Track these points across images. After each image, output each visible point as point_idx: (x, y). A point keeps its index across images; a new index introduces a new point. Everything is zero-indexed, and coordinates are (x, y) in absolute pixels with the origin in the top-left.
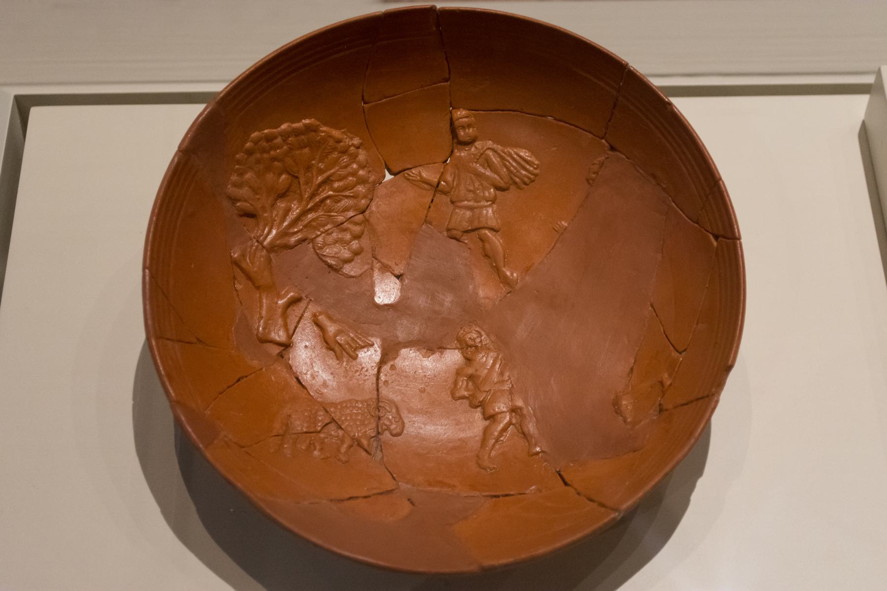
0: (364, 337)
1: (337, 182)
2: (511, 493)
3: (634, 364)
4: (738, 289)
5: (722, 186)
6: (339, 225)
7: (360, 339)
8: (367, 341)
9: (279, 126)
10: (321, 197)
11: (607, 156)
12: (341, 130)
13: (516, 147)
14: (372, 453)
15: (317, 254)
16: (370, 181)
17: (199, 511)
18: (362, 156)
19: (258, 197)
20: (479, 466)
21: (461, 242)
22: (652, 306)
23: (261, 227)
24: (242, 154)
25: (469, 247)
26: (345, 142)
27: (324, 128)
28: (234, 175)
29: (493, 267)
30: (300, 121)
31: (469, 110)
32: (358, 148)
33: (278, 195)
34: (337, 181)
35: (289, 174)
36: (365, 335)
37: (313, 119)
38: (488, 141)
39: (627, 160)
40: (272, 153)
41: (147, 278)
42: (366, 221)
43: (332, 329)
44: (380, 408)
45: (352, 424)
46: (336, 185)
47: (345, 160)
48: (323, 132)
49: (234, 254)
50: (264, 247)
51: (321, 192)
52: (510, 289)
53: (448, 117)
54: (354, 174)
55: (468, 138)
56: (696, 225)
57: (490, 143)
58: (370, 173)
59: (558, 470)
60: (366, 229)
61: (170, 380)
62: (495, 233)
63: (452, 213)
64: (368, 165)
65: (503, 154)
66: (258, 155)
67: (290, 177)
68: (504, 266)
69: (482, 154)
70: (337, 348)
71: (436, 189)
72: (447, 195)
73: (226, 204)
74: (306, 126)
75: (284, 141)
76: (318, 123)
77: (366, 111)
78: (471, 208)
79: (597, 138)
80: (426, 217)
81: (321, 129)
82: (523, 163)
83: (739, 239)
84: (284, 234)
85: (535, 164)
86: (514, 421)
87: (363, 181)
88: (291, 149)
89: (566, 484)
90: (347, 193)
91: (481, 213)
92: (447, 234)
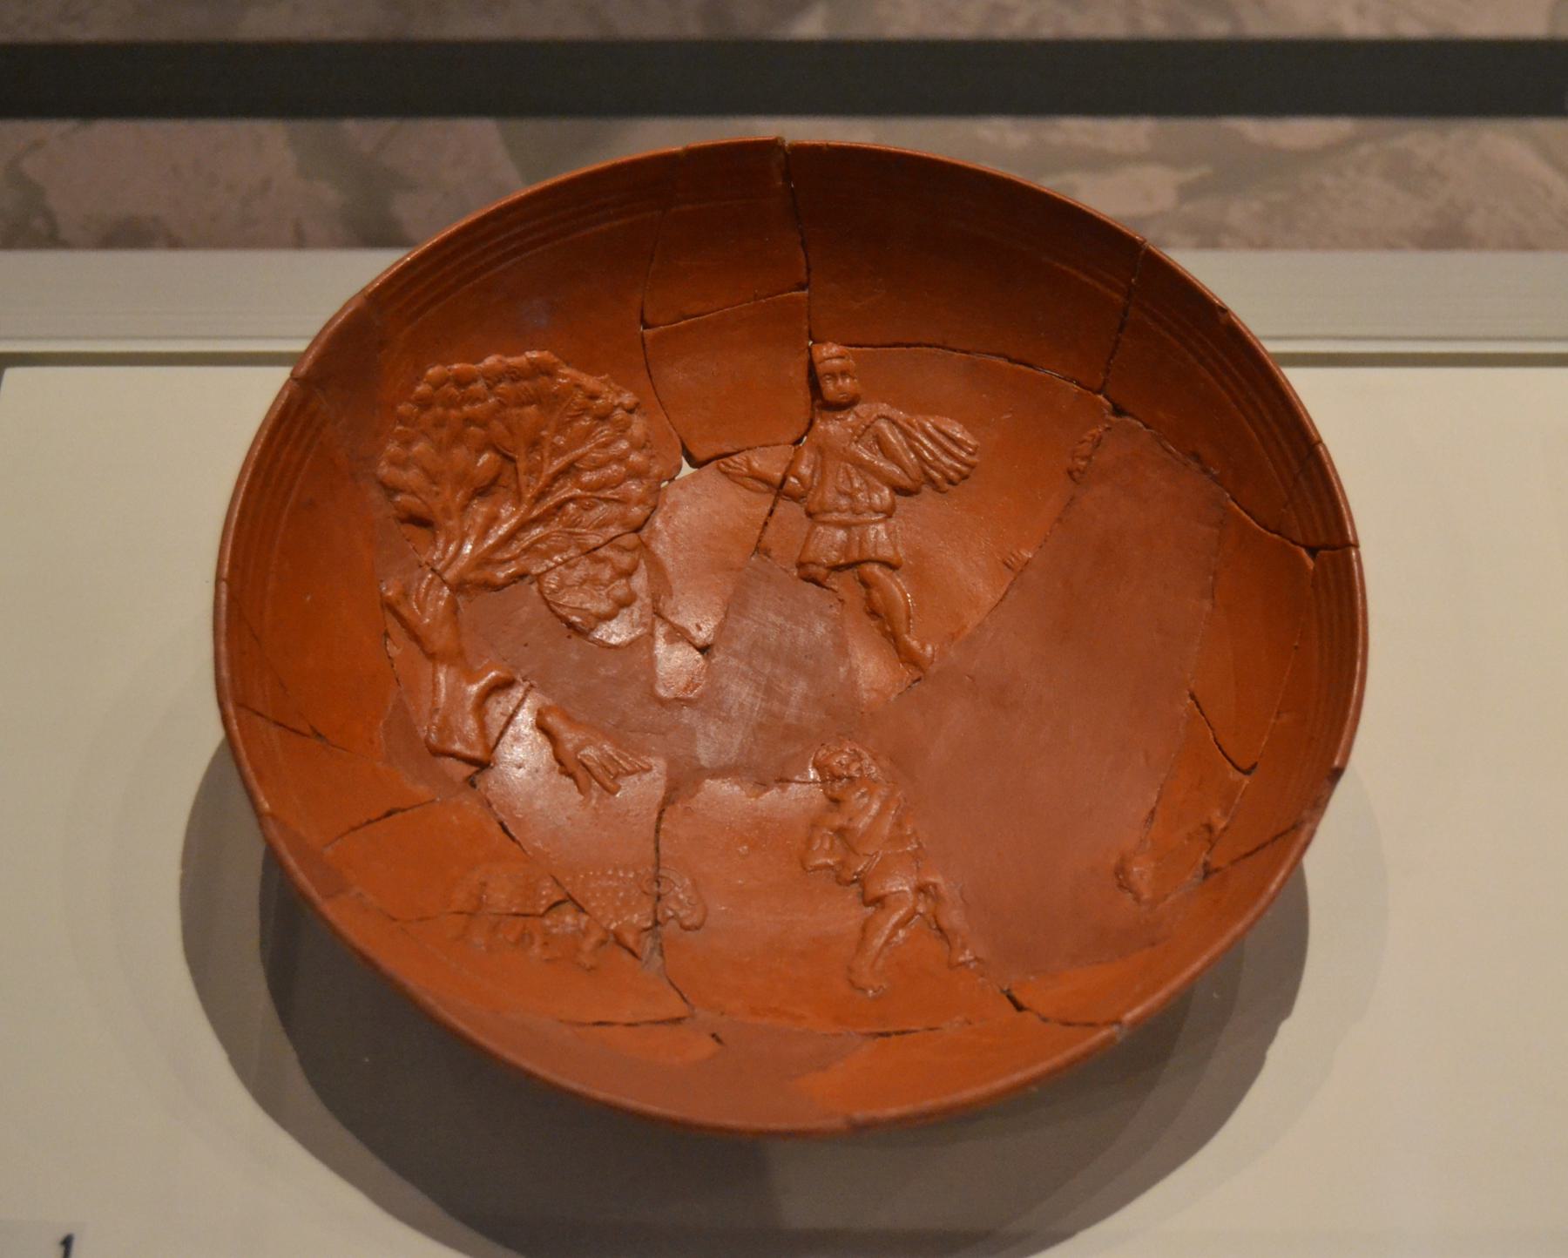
0: (632, 755)
1: (588, 473)
2: (913, 1028)
3: (1157, 802)
4: (1354, 635)
5: (1323, 453)
6: (589, 552)
7: (625, 759)
8: (639, 763)
9: (481, 360)
10: (557, 499)
11: (1107, 426)
12: (599, 375)
13: (933, 413)
14: (644, 959)
15: (547, 603)
16: (651, 474)
17: (302, 1061)
18: (638, 427)
19: (435, 488)
20: (852, 983)
21: (823, 586)
22: (1192, 696)
23: (441, 544)
24: (410, 405)
25: (841, 598)
26: (607, 398)
27: (566, 371)
28: (392, 442)
29: (885, 634)
30: (521, 353)
31: (845, 345)
32: (630, 411)
33: (476, 489)
34: (590, 471)
35: (497, 451)
36: (635, 752)
37: (546, 353)
38: (880, 404)
39: (1145, 429)
40: (466, 408)
41: (224, 597)
42: (644, 546)
43: (570, 738)
44: (660, 880)
45: (604, 904)
46: (587, 477)
47: (606, 432)
48: (565, 377)
49: (388, 589)
50: (445, 582)
51: (557, 490)
52: (917, 674)
53: (805, 358)
54: (621, 459)
55: (841, 396)
56: (1276, 536)
57: (884, 408)
58: (652, 461)
59: (1006, 988)
60: (642, 562)
61: (260, 777)
62: (891, 571)
63: (809, 534)
64: (648, 445)
65: (909, 428)
66: (439, 410)
67: (498, 458)
68: (908, 632)
69: (868, 427)
70: (580, 774)
71: (778, 492)
72: (800, 503)
73: (375, 494)
74: (531, 362)
75: (490, 388)
76: (556, 360)
77: (647, 342)
78: (845, 526)
79: (1090, 392)
80: (759, 541)
81: (561, 371)
82: (948, 444)
83: (1356, 546)
84: (484, 561)
85: (970, 446)
86: (921, 909)
87: (637, 474)
88: (502, 405)
89: (1019, 1008)
90: (608, 493)
91: (863, 536)
92: (799, 572)
